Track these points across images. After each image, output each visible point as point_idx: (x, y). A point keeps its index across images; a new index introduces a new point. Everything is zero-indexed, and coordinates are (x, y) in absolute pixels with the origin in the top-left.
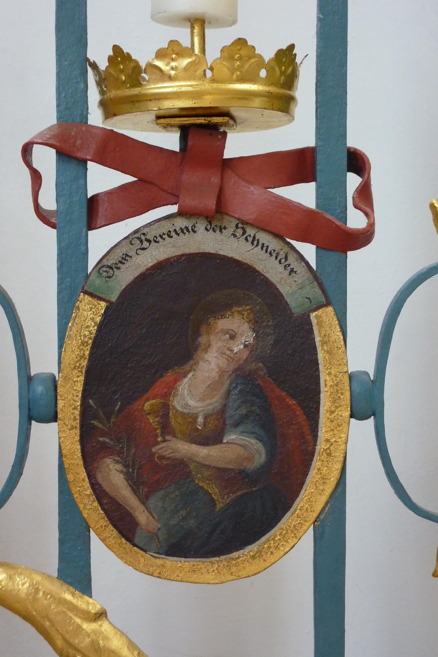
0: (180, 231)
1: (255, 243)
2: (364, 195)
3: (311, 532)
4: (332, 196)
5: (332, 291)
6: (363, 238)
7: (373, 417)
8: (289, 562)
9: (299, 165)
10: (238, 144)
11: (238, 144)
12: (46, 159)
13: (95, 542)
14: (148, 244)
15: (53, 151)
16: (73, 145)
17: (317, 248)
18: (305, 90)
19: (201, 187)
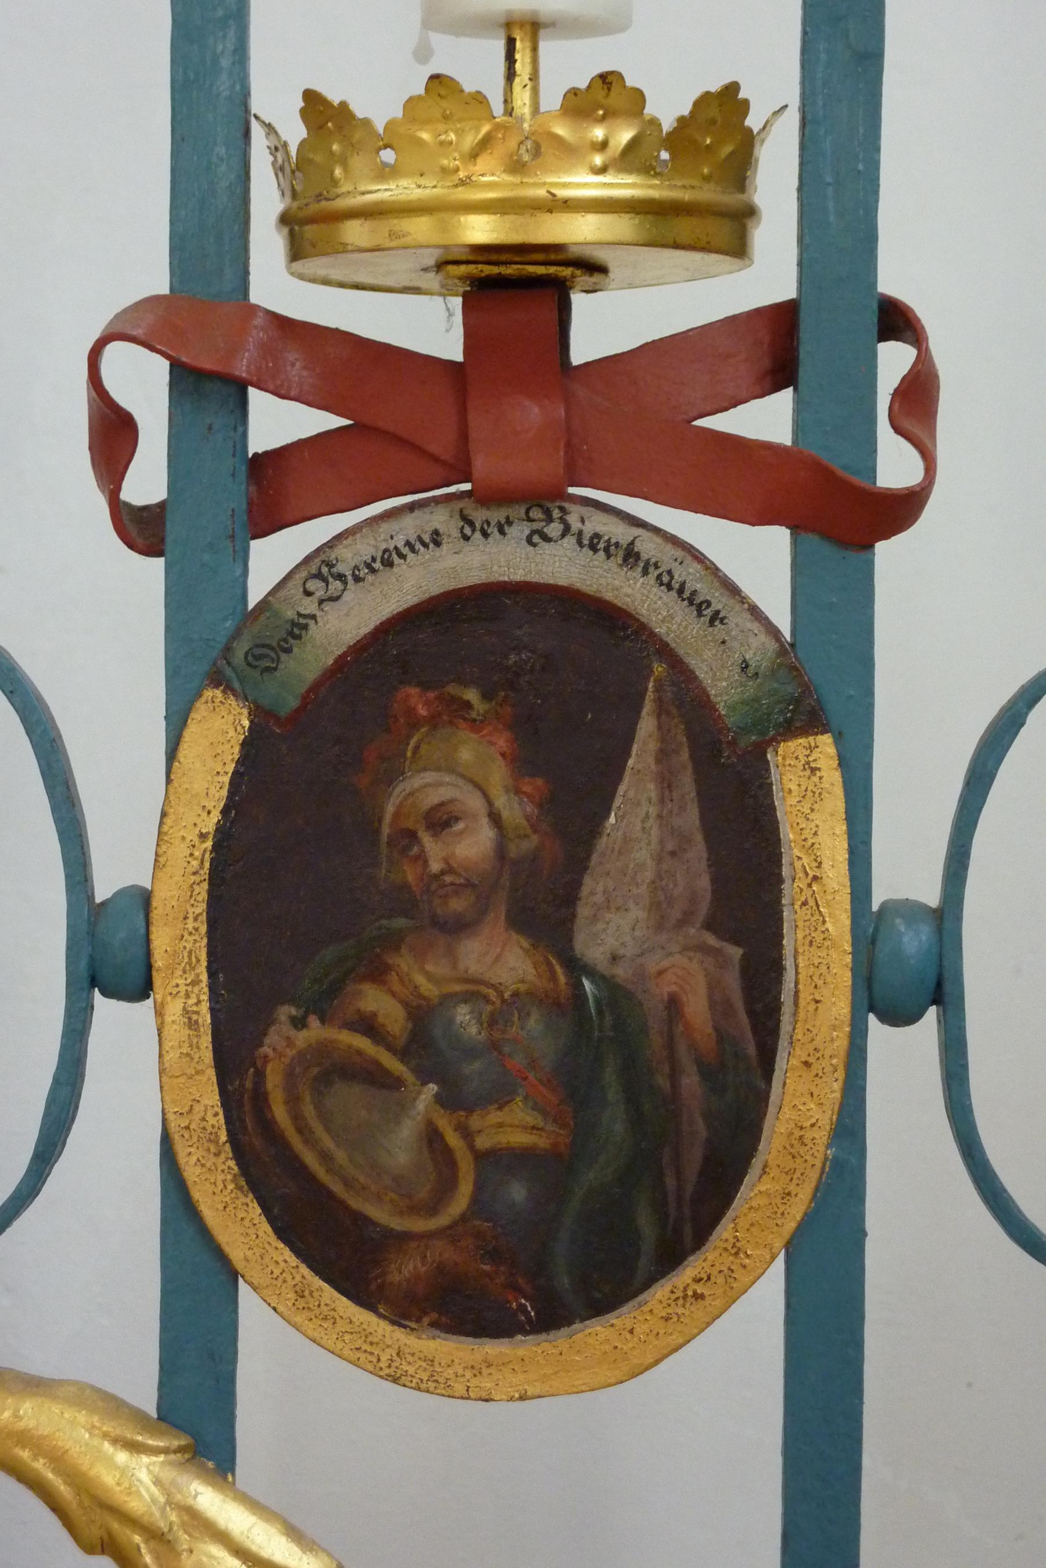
0: (417, 547)
1: (258, 651)
2: (918, 397)
3: (779, 1265)
6: (901, 510)
7: (933, 1010)
8: (720, 1361)
9: (773, 348)
10: (601, 326)
11: (601, 326)
12: (142, 382)
13: (251, 1309)
14: (338, 584)
15: (166, 364)
16: (211, 346)
18: (776, 183)
19: (519, 429)
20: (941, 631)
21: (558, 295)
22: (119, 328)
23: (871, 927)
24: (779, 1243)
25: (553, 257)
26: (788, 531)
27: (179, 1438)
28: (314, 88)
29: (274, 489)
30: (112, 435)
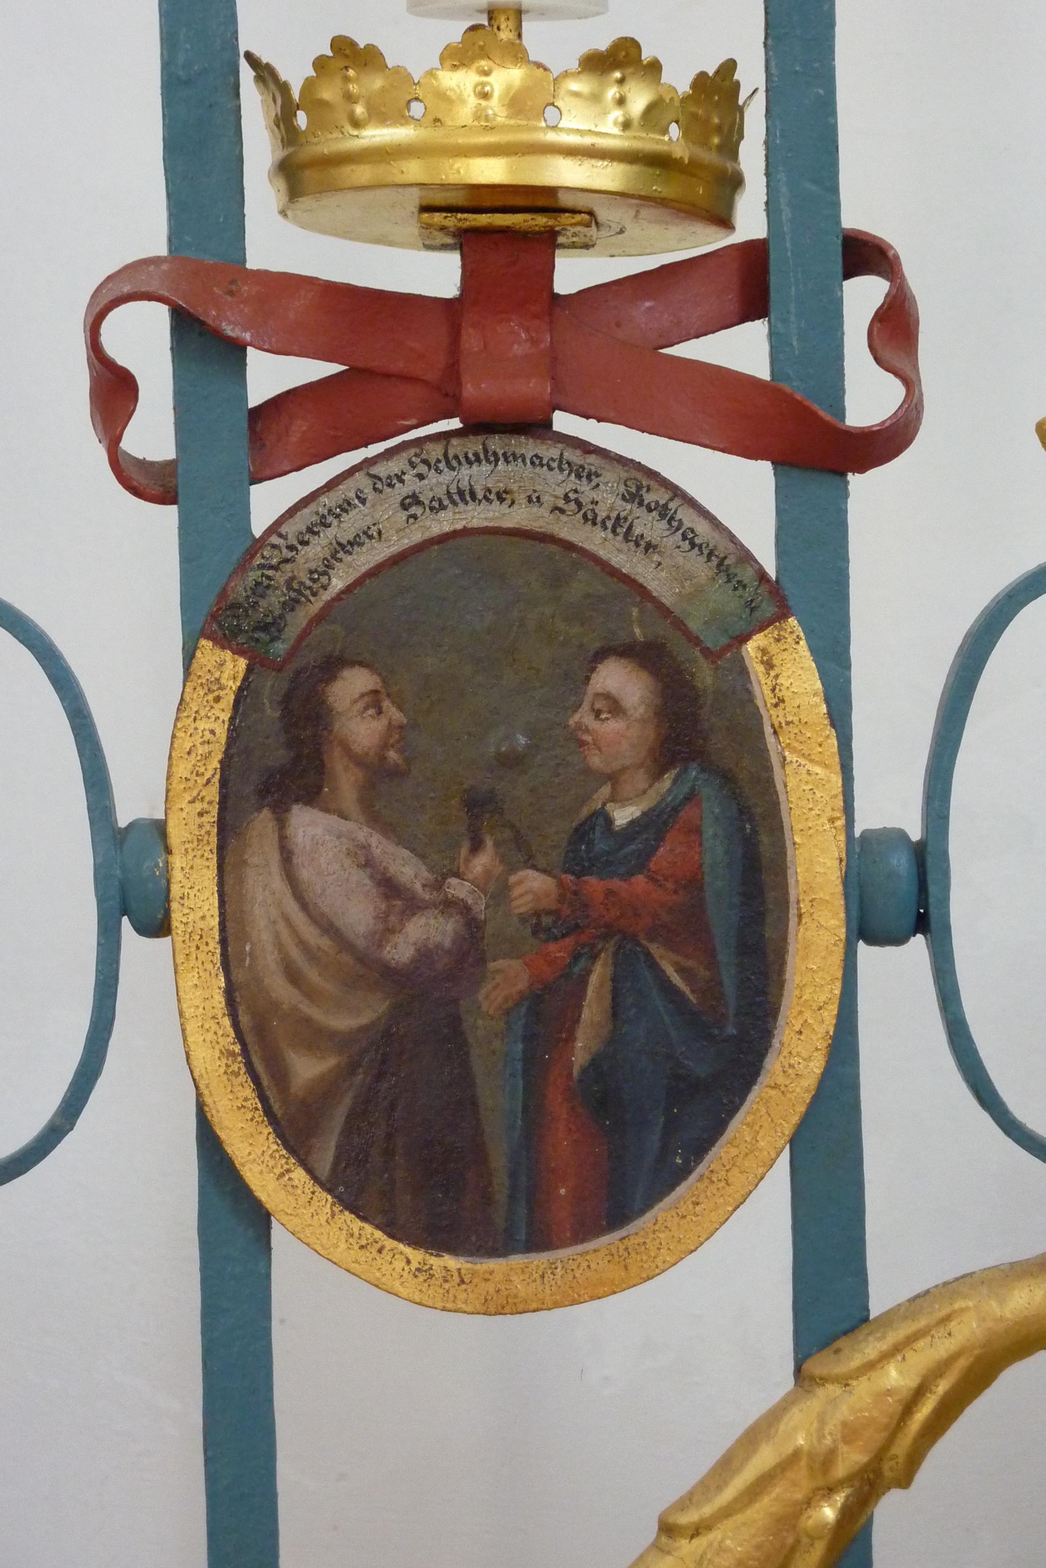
3: (784, 1161)
4: (814, 347)
5: (810, 587)
6: (885, 443)
12: (143, 338)
16: (210, 303)
17: (773, 463)
19: (503, 363)
20: (911, 549)
21: (548, 242)
22: (104, 301)
23: (864, 853)
24: (782, 1141)
25: (541, 202)
26: (769, 463)
27: (254, 859)
28: (383, 49)
29: (275, 434)
30: (114, 392)
